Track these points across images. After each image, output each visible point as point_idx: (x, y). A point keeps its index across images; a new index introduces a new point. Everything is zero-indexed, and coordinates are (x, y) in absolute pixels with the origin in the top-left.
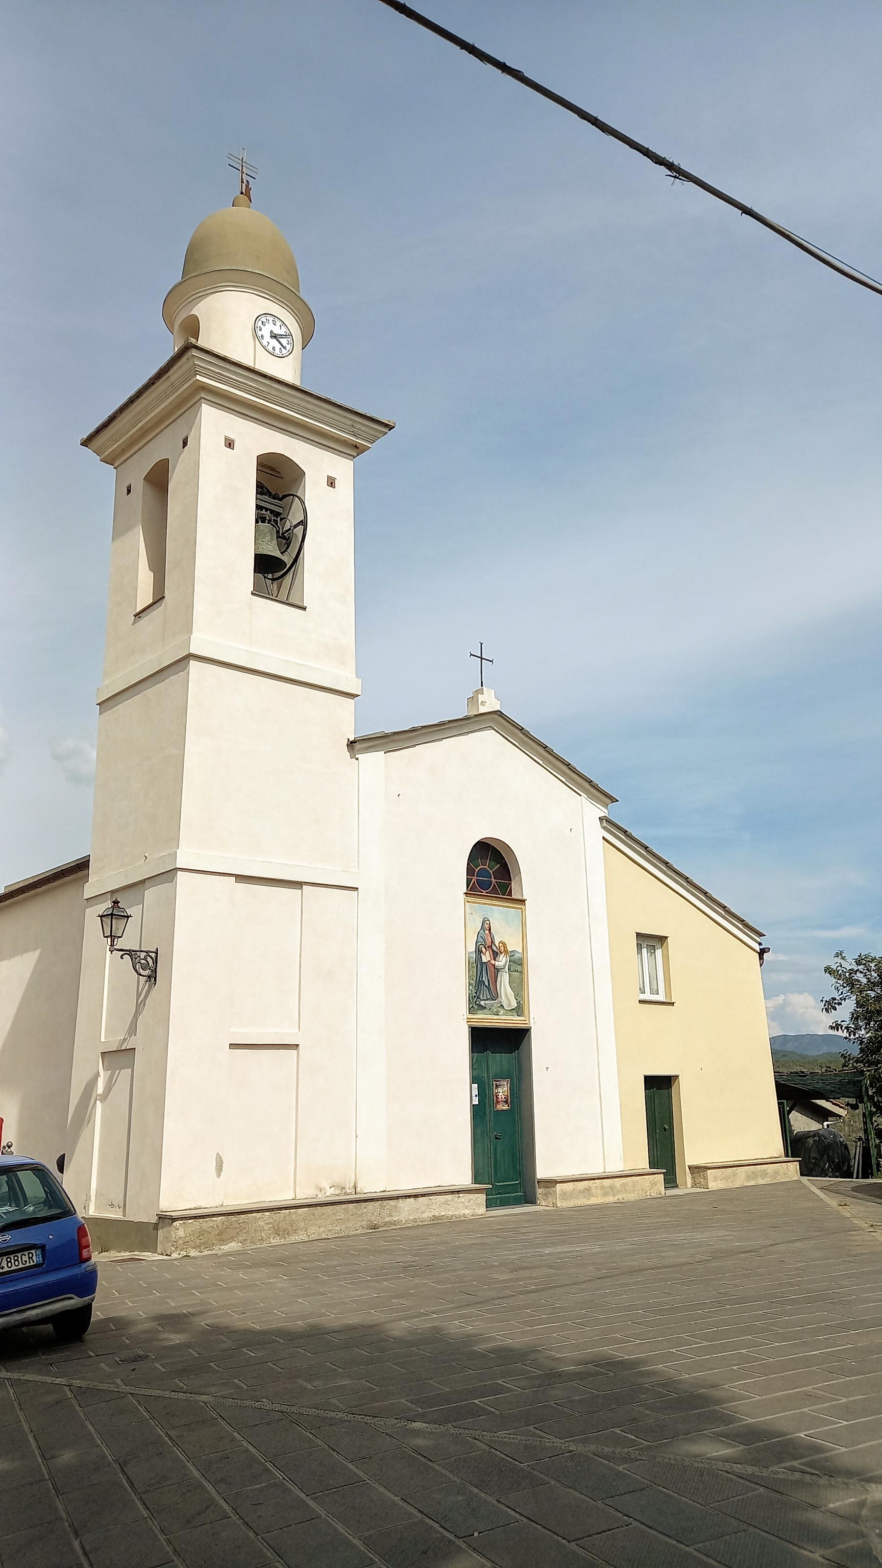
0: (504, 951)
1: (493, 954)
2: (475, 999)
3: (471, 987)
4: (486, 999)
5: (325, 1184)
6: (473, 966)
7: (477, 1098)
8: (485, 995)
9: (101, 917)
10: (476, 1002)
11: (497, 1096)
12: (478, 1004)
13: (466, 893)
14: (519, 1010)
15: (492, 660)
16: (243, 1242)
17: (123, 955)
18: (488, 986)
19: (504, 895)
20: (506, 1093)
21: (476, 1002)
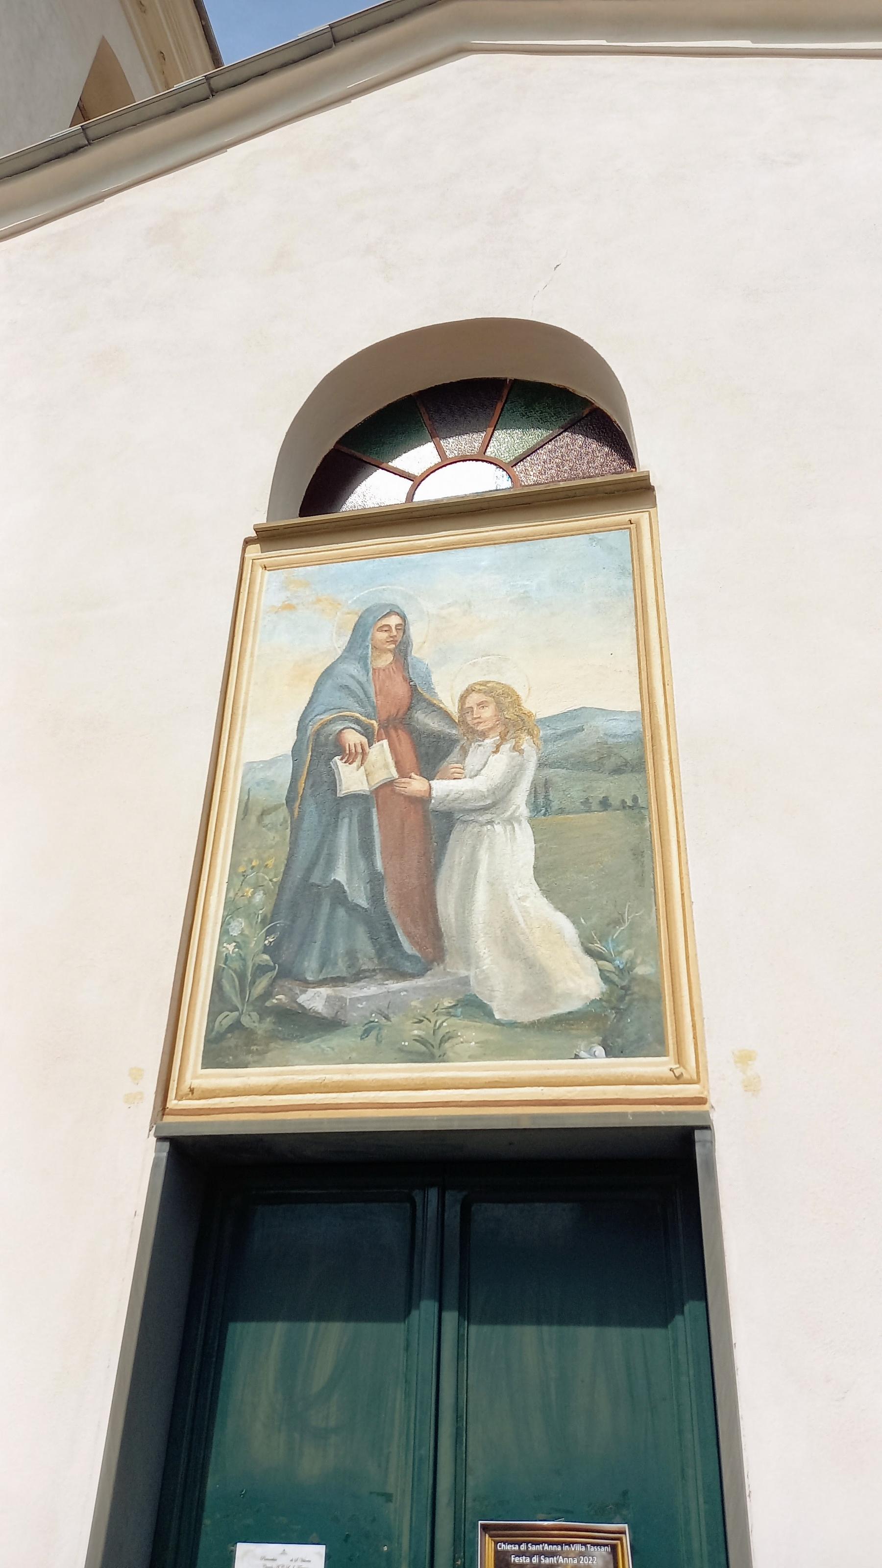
2: (263, 984)
3: (238, 926)
10: (268, 994)
21: (268, 994)
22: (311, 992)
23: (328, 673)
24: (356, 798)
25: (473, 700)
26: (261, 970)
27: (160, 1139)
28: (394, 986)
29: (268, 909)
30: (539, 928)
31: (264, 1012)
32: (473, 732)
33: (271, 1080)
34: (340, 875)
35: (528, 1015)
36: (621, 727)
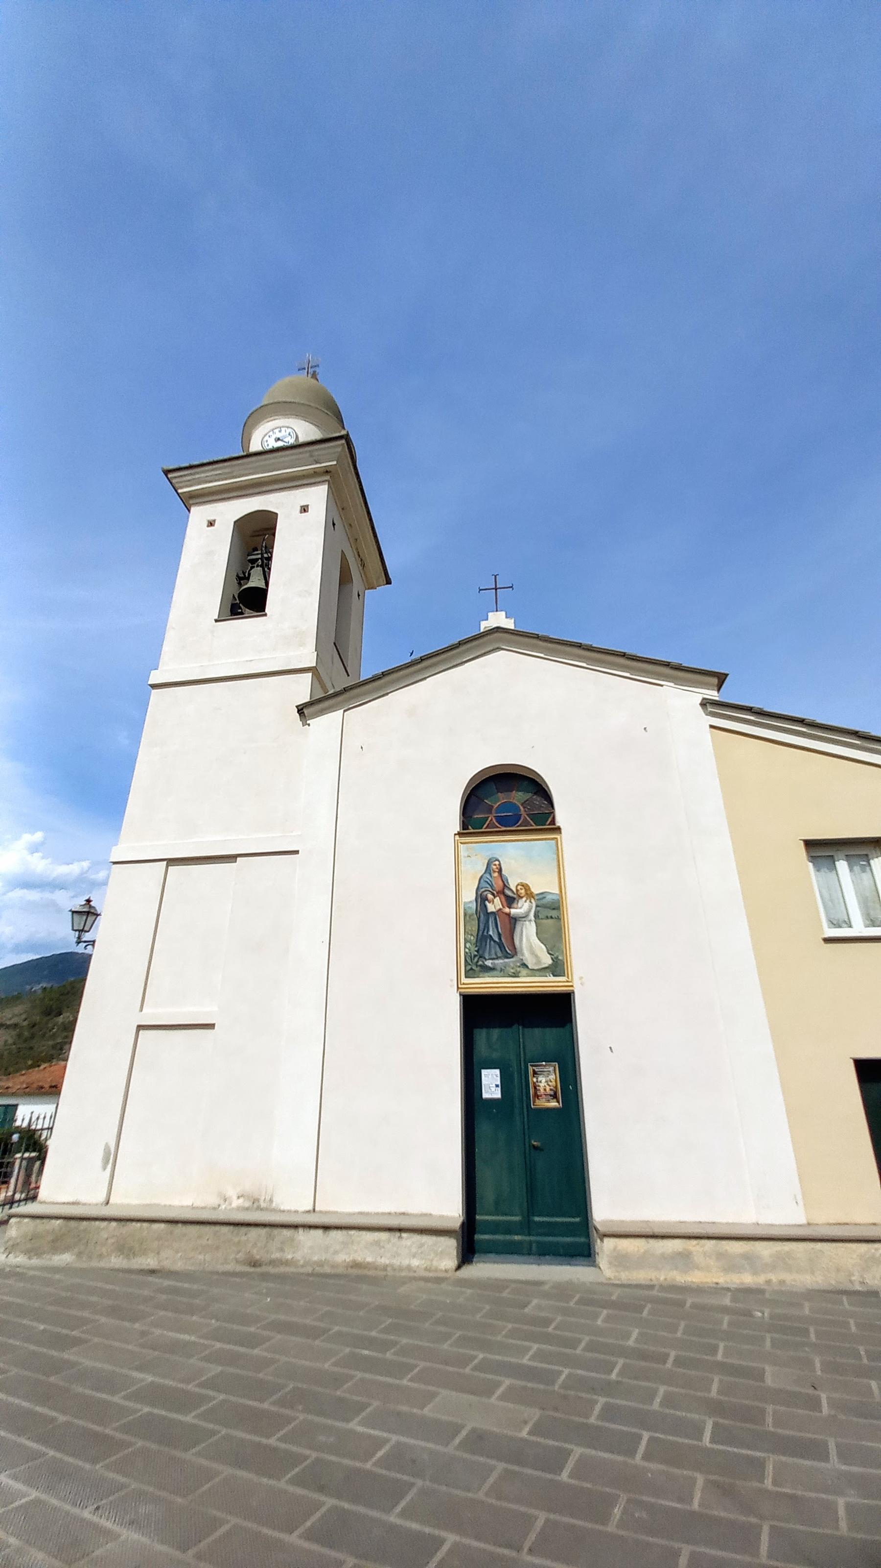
0: (527, 894)
1: (506, 900)
2: (476, 959)
3: (468, 945)
4: (495, 957)
5: (232, 1193)
6: (472, 917)
7: (499, 1089)
8: (493, 951)
9: (73, 912)
10: (477, 962)
11: (535, 1088)
12: (481, 966)
13: (459, 834)
14: (557, 968)
15: (494, 576)
16: (80, 1255)
17: (86, 946)
18: (497, 940)
19: (545, 825)
20: (554, 1083)
21: (477, 962)
22: (488, 961)
23: (481, 877)
24: (492, 913)
25: (519, 887)
26: (475, 956)
27: (460, 995)
28: (506, 960)
29: (475, 940)
30: (27, 1088)
31: (477, 966)
32: (519, 896)
33: (482, 981)
34: (491, 933)
35: (536, 968)
36: (554, 897)
